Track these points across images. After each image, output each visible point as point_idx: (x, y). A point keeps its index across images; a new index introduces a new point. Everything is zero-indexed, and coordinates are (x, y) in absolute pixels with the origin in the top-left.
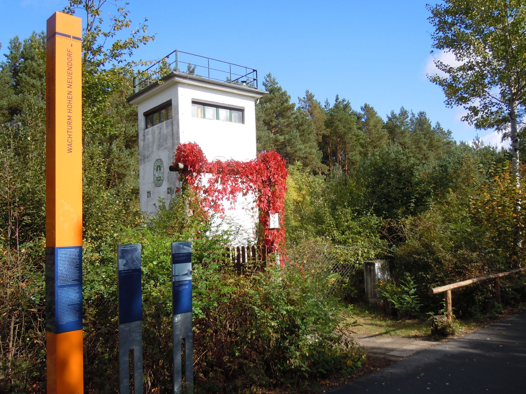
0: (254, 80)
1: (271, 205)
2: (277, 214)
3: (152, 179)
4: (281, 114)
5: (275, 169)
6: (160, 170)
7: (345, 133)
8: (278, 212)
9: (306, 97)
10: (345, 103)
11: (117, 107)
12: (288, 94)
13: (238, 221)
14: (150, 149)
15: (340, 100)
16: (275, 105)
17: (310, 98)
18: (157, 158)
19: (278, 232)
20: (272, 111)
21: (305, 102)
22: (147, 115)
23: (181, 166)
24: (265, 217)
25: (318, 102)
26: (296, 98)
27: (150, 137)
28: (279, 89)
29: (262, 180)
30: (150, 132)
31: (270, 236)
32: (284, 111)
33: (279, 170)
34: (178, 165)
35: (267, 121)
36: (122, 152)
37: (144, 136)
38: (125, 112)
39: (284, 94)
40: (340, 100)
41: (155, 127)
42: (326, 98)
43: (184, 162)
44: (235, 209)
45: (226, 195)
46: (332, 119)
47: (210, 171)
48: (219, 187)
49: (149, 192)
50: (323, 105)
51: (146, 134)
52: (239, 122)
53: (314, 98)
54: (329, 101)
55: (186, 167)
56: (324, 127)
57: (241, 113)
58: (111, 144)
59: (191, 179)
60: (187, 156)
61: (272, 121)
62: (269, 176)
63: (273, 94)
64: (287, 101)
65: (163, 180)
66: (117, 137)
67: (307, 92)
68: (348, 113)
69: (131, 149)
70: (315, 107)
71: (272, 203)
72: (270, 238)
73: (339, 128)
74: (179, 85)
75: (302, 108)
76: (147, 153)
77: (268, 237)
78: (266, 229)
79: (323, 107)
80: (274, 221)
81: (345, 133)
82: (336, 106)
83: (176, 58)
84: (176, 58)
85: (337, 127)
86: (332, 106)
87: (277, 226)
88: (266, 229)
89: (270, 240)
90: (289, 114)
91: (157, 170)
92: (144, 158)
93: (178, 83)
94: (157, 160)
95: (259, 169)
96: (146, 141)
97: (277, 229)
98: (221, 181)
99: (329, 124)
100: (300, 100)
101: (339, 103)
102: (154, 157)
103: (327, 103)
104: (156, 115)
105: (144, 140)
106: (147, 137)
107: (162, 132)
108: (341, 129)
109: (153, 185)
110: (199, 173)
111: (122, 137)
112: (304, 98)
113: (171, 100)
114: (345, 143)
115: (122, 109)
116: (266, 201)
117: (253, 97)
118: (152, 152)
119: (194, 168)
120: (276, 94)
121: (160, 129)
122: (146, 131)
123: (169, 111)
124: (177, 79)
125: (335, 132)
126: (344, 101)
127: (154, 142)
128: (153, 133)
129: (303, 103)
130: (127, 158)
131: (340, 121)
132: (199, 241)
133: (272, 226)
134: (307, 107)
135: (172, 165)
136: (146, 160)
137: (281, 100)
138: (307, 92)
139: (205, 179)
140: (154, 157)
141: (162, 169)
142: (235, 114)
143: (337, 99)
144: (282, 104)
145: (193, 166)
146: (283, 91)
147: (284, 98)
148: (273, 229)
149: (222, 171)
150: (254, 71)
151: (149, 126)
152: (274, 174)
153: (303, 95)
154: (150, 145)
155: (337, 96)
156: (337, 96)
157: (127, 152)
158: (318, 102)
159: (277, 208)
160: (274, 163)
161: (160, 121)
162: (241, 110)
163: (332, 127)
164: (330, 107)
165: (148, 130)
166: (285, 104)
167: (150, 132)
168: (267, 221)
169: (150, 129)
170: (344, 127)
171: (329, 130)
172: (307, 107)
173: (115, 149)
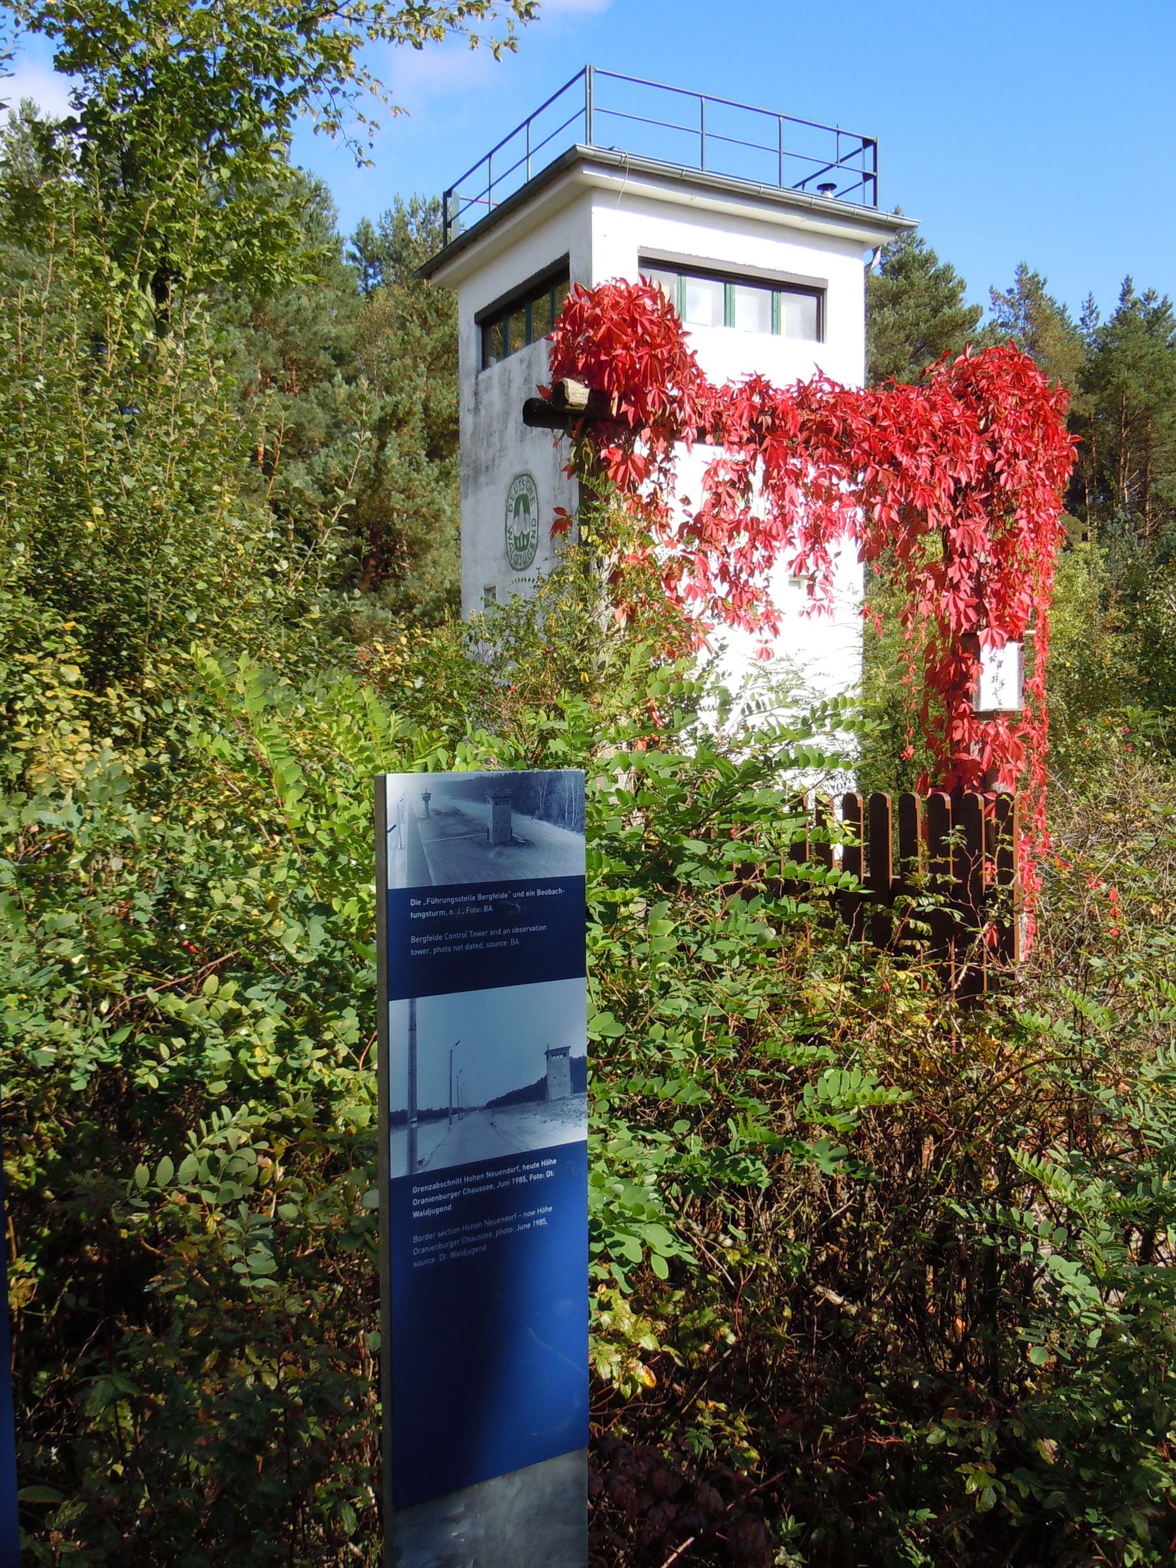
0: (867, 177)
1: (989, 603)
2: (1013, 648)
3: (501, 546)
4: (932, 344)
5: (1017, 429)
6: (527, 510)
7: (1148, 408)
8: (1020, 639)
9: (1015, 287)
10: (1154, 305)
11: (403, 327)
12: (958, 273)
13: (819, 684)
14: (496, 439)
15: (1137, 294)
16: (910, 315)
17: (1030, 289)
18: (518, 469)
19: (1012, 729)
20: (902, 335)
21: (1012, 306)
22: (487, 320)
23: (578, 393)
24: (955, 656)
25: (1059, 304)
26: (982, 290)
27: (494, 396)
28: (929, 260)
29: (957, 481)
30: (495, 381)
31: (975, 748)
32: (941, 334)
33: (1038, 433)
34: (559, 390)
35: (882, 370)
36: (417, 471)
37: (476, 394)
38: (426, 340)
39: (944, 275)
40: (1137, 294)
41: (513, 359)
42: (1085, 293)
43: (590, 375)
44: (830, 612)
45: (790, 542)
46: (1105, 359)
47: (715, 430)
48: (761, 506)
49: (490, 590)
50: (1075, 315)
51: (482, 386)
52: (806, 336)
53: (1047, 291)
54: (1096, 302)
55: (599, 397)
56: (1075, 389)
57: (812, 301)
58: (382, 446)
59: (624, 461)
60: (609, 340)
61: (898, 370)
62: (991, 466)
63: (907, 277)
64: (952, 298)
65: (534, 547)
66: (401, 423)
67: (1022, 269)
68: (1164, 338)
69: (442, 458)
70: (1048, 319)
71: (996, 593)
72: (975, 755)
73: (1128, 393)
74: (596, 197)
75: (1003, 325)
76: (484, 456)
77: (967, 750)
78: (962, 715)
79: (1076, 321)
80: (999, 680)
81: (1148, 408)
82: (1122, 318)
83: (588, 97)
84: (588, 97)
85: (1121, 388)
86: (1107, 312)
87: (1011, 700)
88: (962, 715)
89: (976, 765)
90: (957, 340)
91: (517, 513)
92: (477, 471)
93: (589, 191)
94: (518, 477)
95: (945, 427)
96: (483, 412)
97: (1009, 715)
98: (767, 476)
99: (1094, 378)
100: (995, 297)
101: (1134, 304)
102: (508, 467)
103: (1091, 310)
104: (515, 325)
105: (476, 410)
106: (485, 398)
107: (534, 376)
108: (1137, 393)
109: (504, 564)
110: (668, 431)
111: (416, 422)
112: (1010, 291)
113: (566, 257)
114: (1145, 444)
115: (418, 332)
116: (967, 585)
117: (861, 243)
118: (502, 449)
119: (640, 403)
120: (916, 275)
121: (529, 366)
122: (482, 376)
123: (557, 299)
124: (589, 174)
125: (1114, 409)
126: (1149, 298)
127: (507, 413)
128: (506, 384)
129: (1005, 308)
130: (433, 490)
131: (1131, 367)
132: (652, 759)
133: (987, 703)
134: (1020, 323)
135: (536, 395)
136: (482, 479)
137: (933, 298)
138: (1022, 269)
139: (690, 472)
140: (508, 467)
141: (533, 508)
142: (794, 307)
143: (1126, 291)
144: (936, 311)
145: (633, 393)
146: (941, 264)
147: (942, 289)
148: (992, 715)
149: (772, 429)
150: (867, 143)
151: (492, 359)
152: (1015, 455)
153: (1007, 282)
154: (496, 426)
155: (1128, 280)
156: (1128, 280)
157: (433, 470)
158: (1059, 304)
159: (1014, 616)
160: (1012, 401)
161: (529, 339)
162: (817, 291)
163: (1105, 388)
164: (1100, 324)
165: (488, 372)
166: (946, 310)
167: (495, 381)
168: (966, 677)
169: (496, 367)
170: (1148, 388)
171: (1092, 399)
172: (1020, 323)
173: (395, 461)
